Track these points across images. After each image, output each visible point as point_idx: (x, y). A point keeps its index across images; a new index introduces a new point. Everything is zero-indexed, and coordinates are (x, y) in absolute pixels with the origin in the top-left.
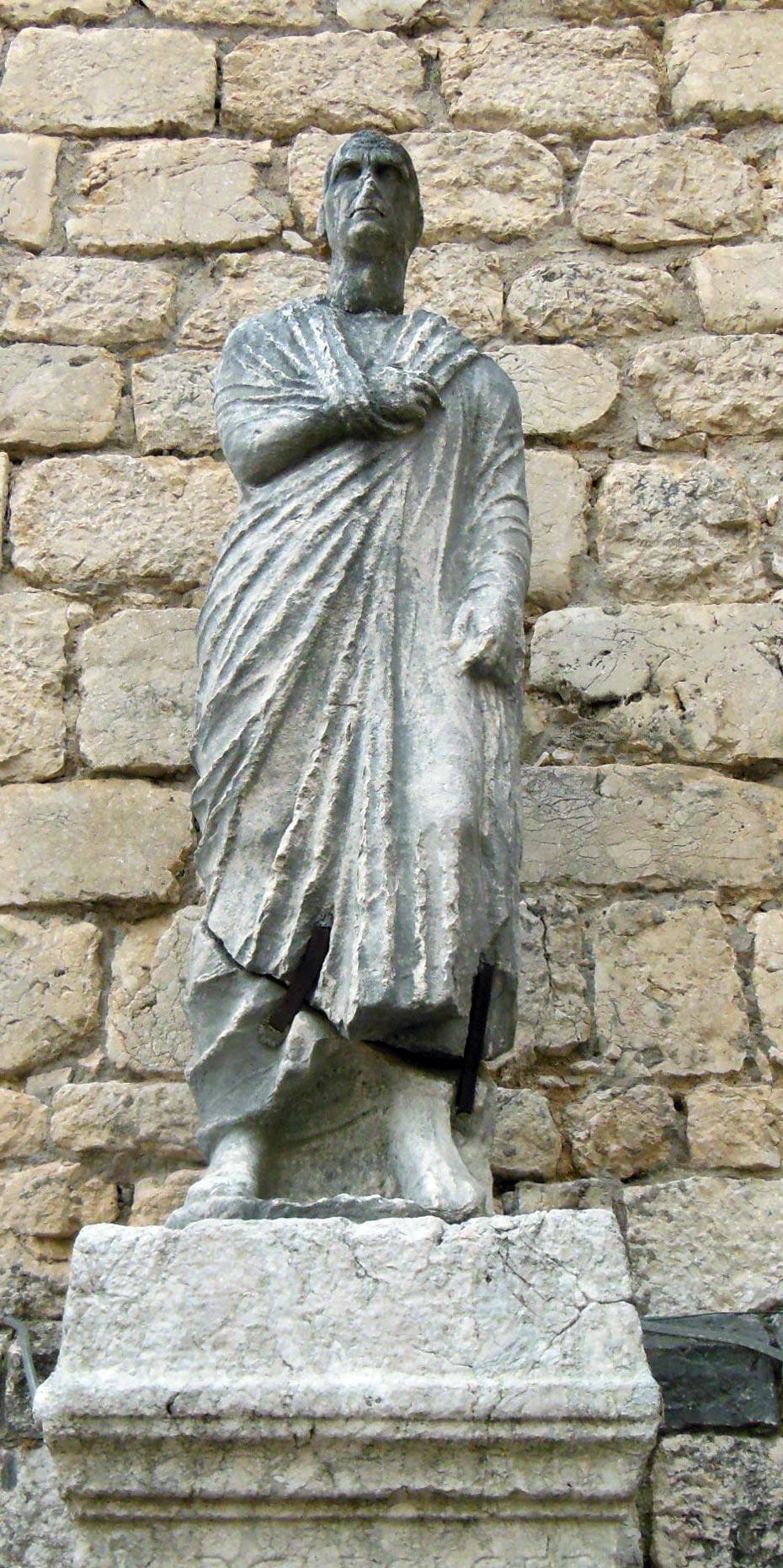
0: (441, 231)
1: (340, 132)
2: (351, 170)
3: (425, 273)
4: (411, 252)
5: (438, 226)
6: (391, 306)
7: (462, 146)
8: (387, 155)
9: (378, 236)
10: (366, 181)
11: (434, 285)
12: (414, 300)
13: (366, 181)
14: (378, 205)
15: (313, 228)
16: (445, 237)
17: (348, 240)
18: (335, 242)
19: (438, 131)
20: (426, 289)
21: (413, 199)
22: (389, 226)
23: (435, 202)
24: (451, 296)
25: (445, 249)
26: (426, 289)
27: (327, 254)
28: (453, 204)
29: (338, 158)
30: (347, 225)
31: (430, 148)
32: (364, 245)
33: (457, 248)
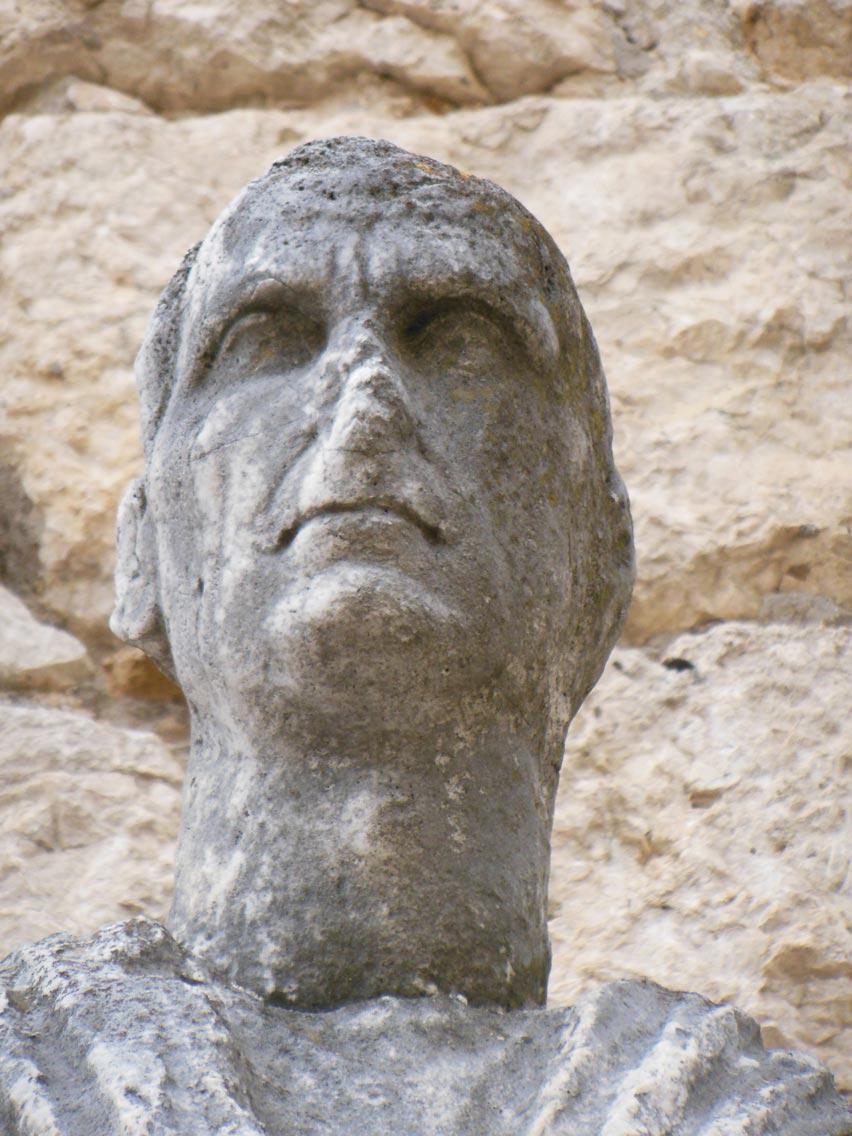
0: (712, 566)
1: (210, 104)
2: (280, 324)
3: (638, 775)
4: (578, 695)
5: (699, 542)
6: (490, 969)
7: (801, 158)
8: (450, 252)
9: (419, 634)
10: (352, 374)
11: (683, 826)
12: (596, 922)
13: (352, 374)
14: (409, 491)
15: (86, 567)
16: (729, 596)
17: (269, 659)
18: (209, 666)
19: (679, 87)
20: (649, 850)
21: (580, 446)
22: (473, 587)
23: (675, 424)
24: (770, 880)
25: (733, 653)
26: (649, 850)
27: (154, 690)
28: (767, 433)
29: (213, 272)
30: (263, 589)
31: (651, 171)
32: (343, 681)
33: (791, 648)
